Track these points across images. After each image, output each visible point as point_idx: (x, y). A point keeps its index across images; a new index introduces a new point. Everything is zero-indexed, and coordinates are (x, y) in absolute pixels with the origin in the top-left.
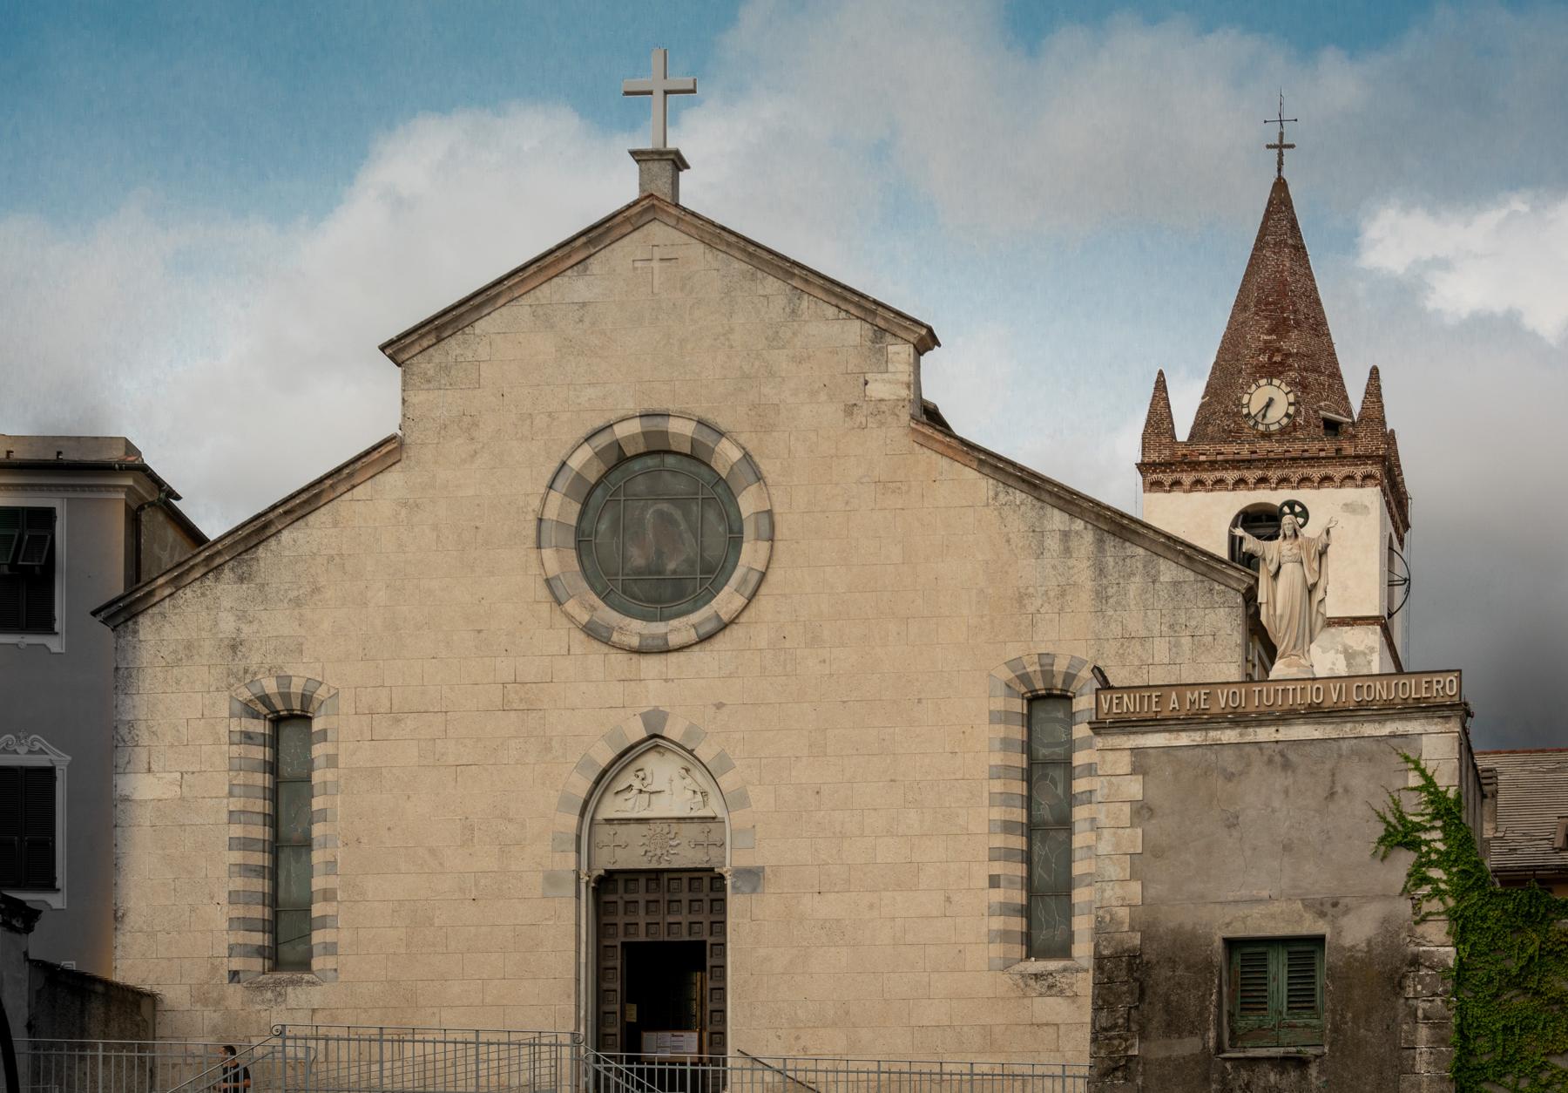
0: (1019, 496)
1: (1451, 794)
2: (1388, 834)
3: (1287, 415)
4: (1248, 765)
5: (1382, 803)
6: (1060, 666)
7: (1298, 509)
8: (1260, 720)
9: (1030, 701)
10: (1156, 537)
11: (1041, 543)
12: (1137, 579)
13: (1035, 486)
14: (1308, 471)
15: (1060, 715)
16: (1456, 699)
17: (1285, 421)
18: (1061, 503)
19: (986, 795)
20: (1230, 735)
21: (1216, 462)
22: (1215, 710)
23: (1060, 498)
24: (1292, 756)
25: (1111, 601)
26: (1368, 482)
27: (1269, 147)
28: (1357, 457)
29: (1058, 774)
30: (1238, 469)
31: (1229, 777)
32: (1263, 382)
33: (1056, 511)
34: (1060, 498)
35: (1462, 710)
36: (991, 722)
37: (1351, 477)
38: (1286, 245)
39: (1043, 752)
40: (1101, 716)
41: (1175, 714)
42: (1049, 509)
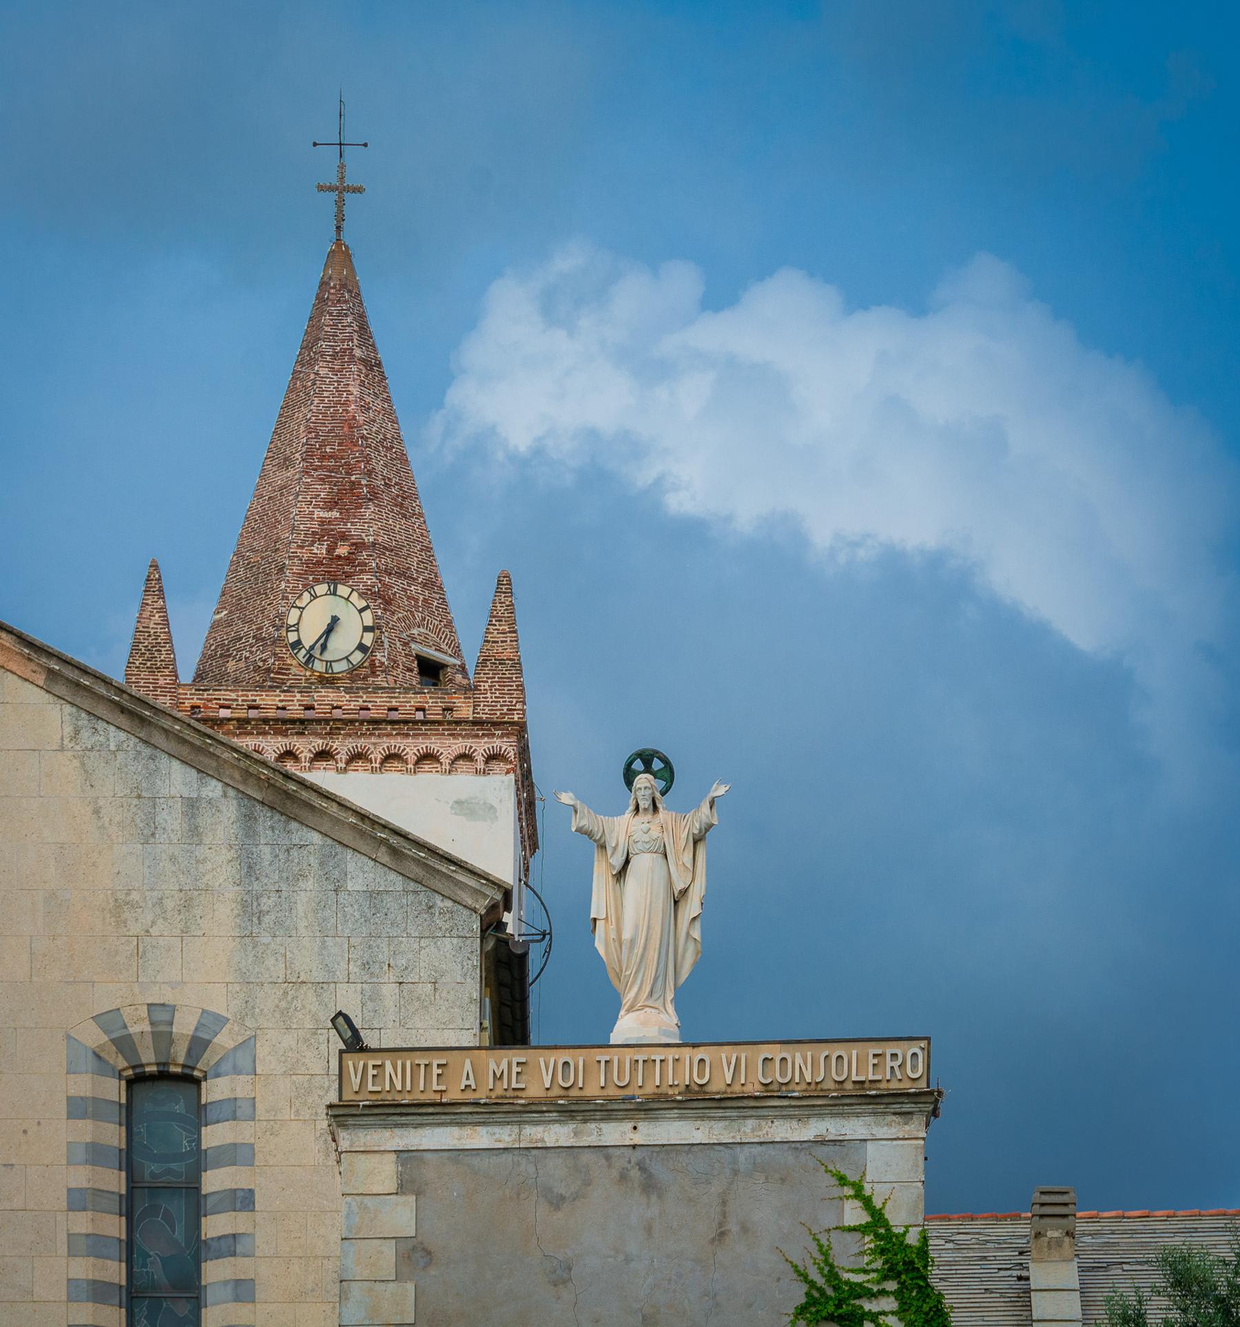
0: (114, 737)
1: (912, 1239)
2: (811, 1302)
3: (362, 647)
4: (587, 1183)
5: (802, 1252)
6: (184, 1026)
7: (657, 765)
8: (607, 1110)
9: (130, 1083)
10: (342, 815)
11: (151, 816)
12: (310, 884)
13: (143, 720)
14: (397, 743)
15: (179, 1108)
16: (922, 1085)
17: (357, 657)
18: (184, 751)
19: (62, 1237)
20: (558, 1134)
21: (247, 721)
22: (534, 1091)
23: (184, 741)
24: (657, 1169)
25: (267, 919)
26: (495, 765)
27: (321, 188)
28: (476, 723)
29: (177, 1206)
30: (284, 734)
31: (557, 1202)
32: (321, 589)
33: (176, 764)
34: (184, 741)
35: (924, 1101)
36: (71, 1115)
37: (466, 757)
38: (352, 356)
39: (150, 1169)
40: (348, 1096)
41: (470, 1096)
42: (164, 759)
